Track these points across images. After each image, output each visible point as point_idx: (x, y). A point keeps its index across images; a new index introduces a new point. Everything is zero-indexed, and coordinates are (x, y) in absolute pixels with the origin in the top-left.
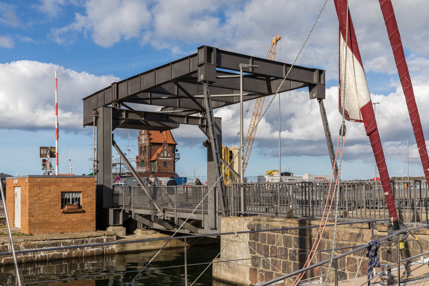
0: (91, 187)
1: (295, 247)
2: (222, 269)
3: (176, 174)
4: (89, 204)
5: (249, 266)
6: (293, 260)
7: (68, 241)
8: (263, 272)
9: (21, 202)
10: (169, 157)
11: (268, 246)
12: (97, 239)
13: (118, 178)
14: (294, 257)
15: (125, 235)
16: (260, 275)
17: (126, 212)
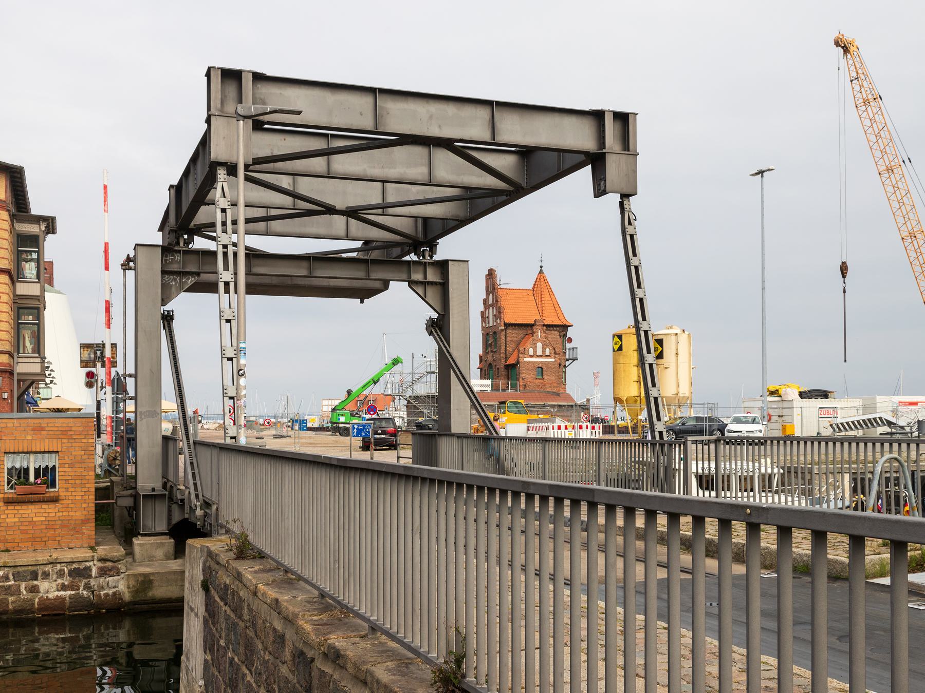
3: (569, 395)
4: (78, 482)
10: (548, 356)
12: (75, 568)
13: (372, 407)
15: (173, 557)
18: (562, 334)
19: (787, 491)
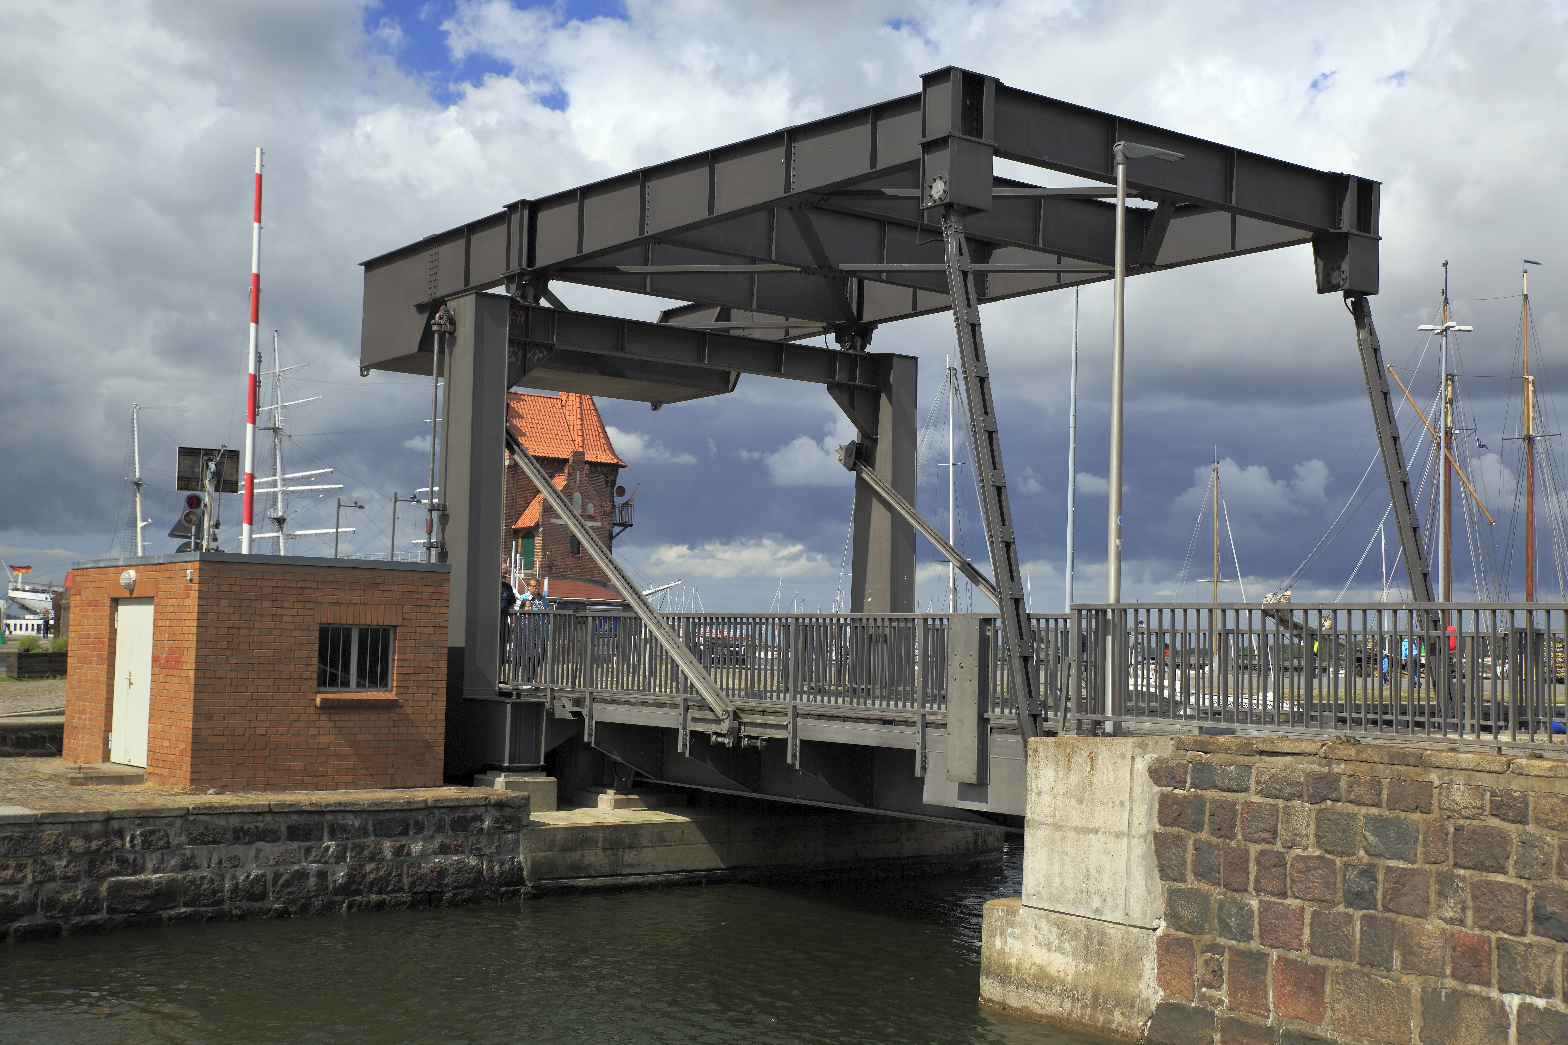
0: (433, 610)
1: (1370, 855)
2: (1032, 940)
5: (1155, 930)
6: (1359, 907)
7: (350, 822)
8: (1222, 954)
9: (155, 659)
11: (1248, 851)
12: (459, 818)
14: (1364, 892)
16: (1207, 962)
17: (556, 716)
18: (610, 480)
19: (1410, 711)
